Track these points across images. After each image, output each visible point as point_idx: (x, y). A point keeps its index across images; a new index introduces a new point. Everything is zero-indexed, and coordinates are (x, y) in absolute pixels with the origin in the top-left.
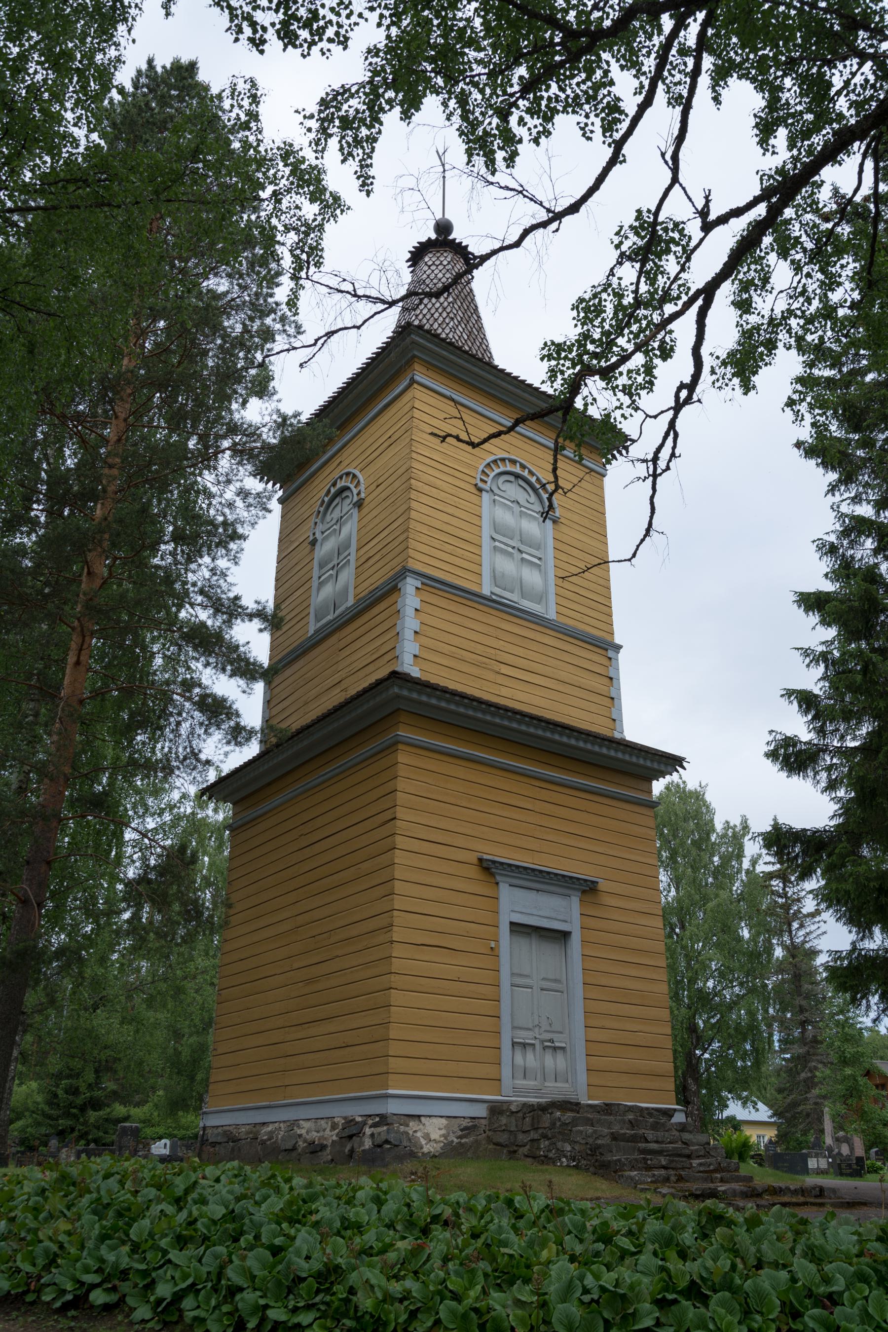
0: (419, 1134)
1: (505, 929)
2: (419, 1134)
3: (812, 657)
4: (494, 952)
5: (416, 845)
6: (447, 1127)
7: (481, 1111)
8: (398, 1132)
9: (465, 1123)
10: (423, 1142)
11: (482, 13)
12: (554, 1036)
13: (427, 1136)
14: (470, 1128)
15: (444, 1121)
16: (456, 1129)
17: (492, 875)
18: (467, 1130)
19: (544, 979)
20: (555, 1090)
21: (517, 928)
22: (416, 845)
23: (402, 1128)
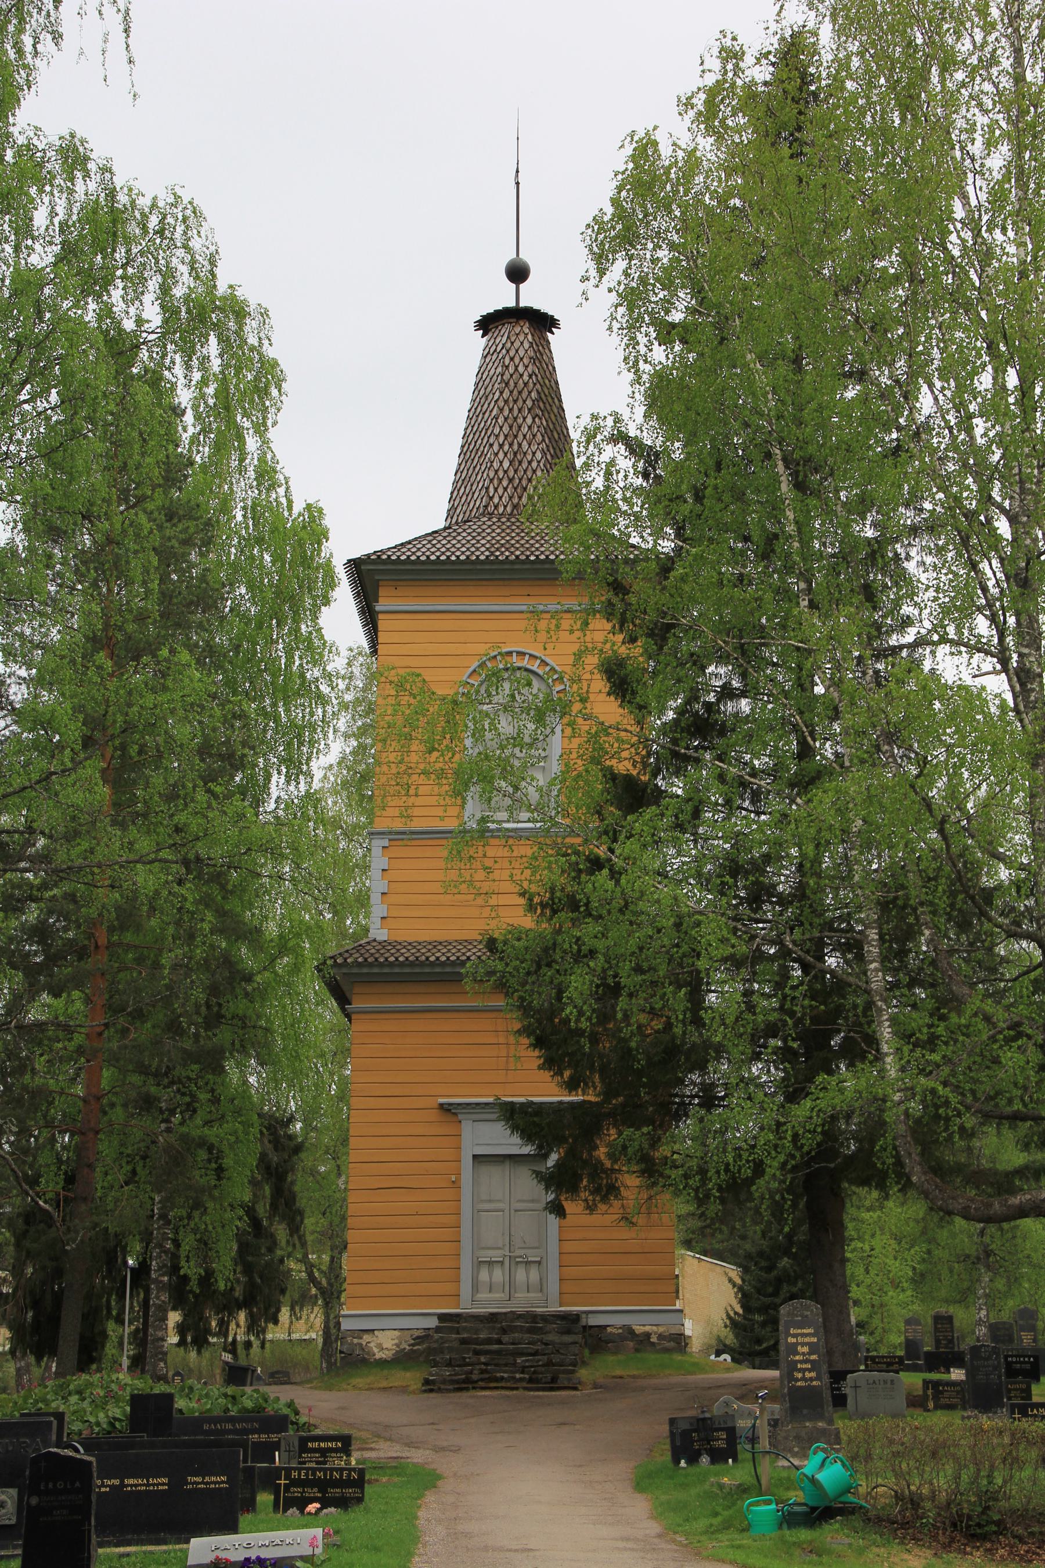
0: (372, 1345)
1: (467, 1162)
2: (372, 1345)
3: (540, 1057)
4: (456, 1185)
5: (372, 1103)
6: (398, 1338)
7: (433, 1323)
8: (352, 1343)
9: (417, 1334)
10: (376, 1350)
11: (216, 1193)
12: (528, 1252)
13: (381, 1348)
14: (424, 1337)
15: (397, 1333)
16: (408, 1338)
17: (455, 1114)
18: (419, 1340)
19: (519, 1201)
20: (523, 1301)
21: (478, 1159)
22: (372, 1103)
23: (356, 1341)
